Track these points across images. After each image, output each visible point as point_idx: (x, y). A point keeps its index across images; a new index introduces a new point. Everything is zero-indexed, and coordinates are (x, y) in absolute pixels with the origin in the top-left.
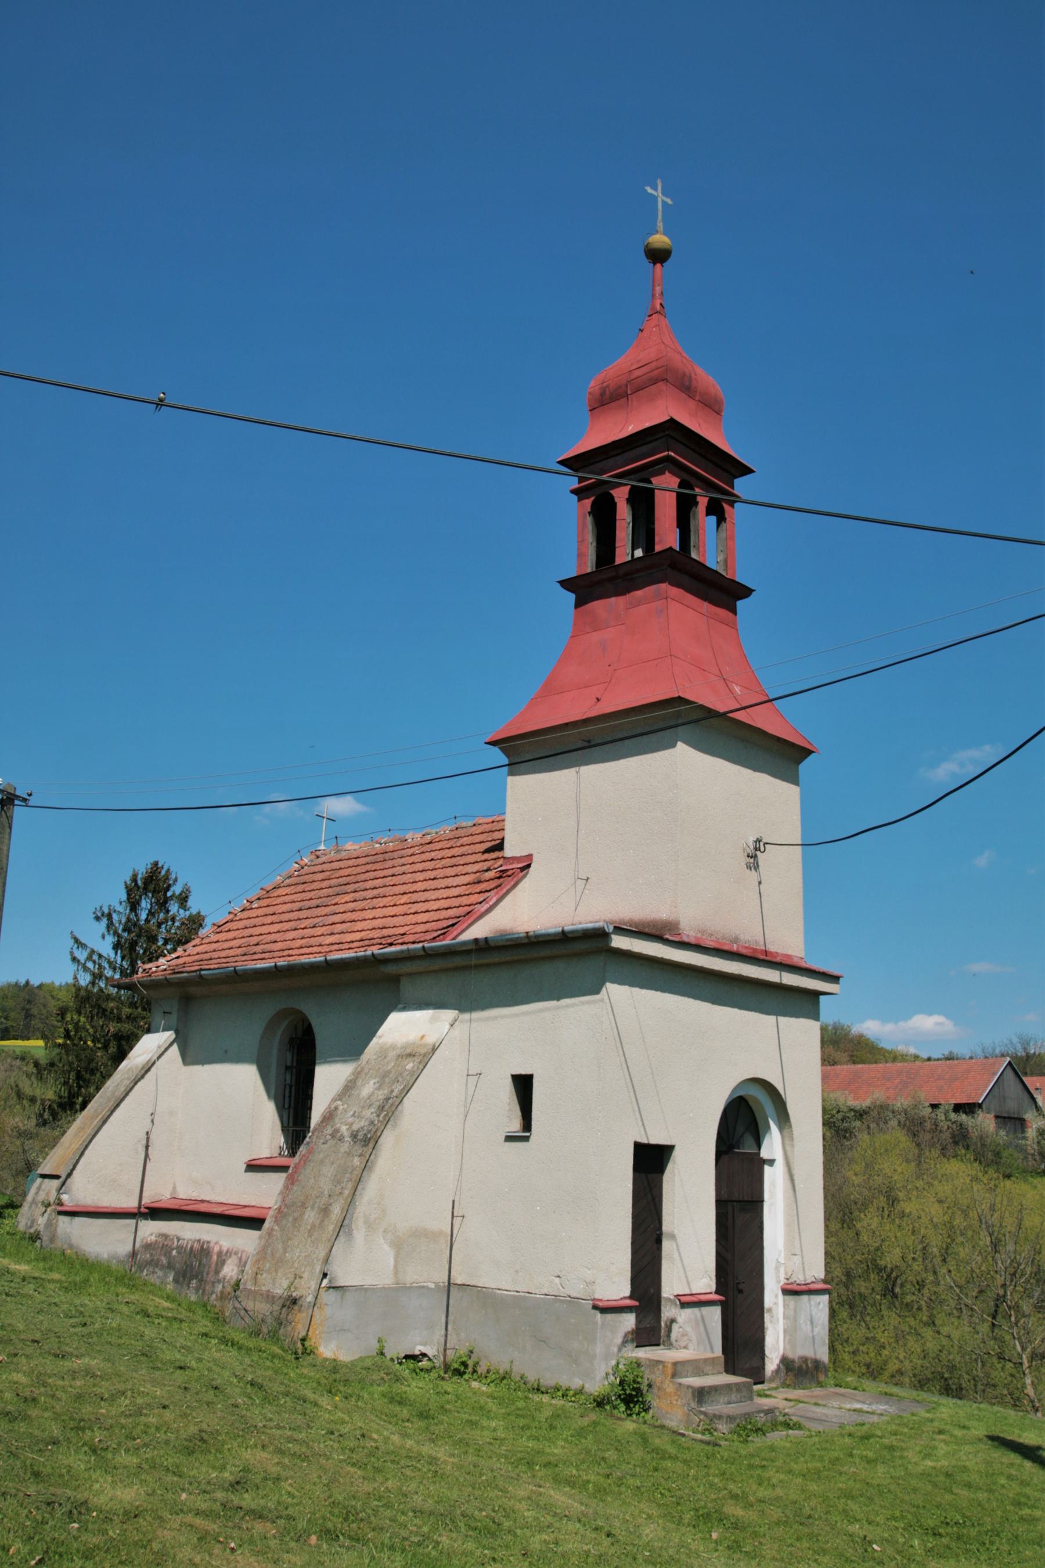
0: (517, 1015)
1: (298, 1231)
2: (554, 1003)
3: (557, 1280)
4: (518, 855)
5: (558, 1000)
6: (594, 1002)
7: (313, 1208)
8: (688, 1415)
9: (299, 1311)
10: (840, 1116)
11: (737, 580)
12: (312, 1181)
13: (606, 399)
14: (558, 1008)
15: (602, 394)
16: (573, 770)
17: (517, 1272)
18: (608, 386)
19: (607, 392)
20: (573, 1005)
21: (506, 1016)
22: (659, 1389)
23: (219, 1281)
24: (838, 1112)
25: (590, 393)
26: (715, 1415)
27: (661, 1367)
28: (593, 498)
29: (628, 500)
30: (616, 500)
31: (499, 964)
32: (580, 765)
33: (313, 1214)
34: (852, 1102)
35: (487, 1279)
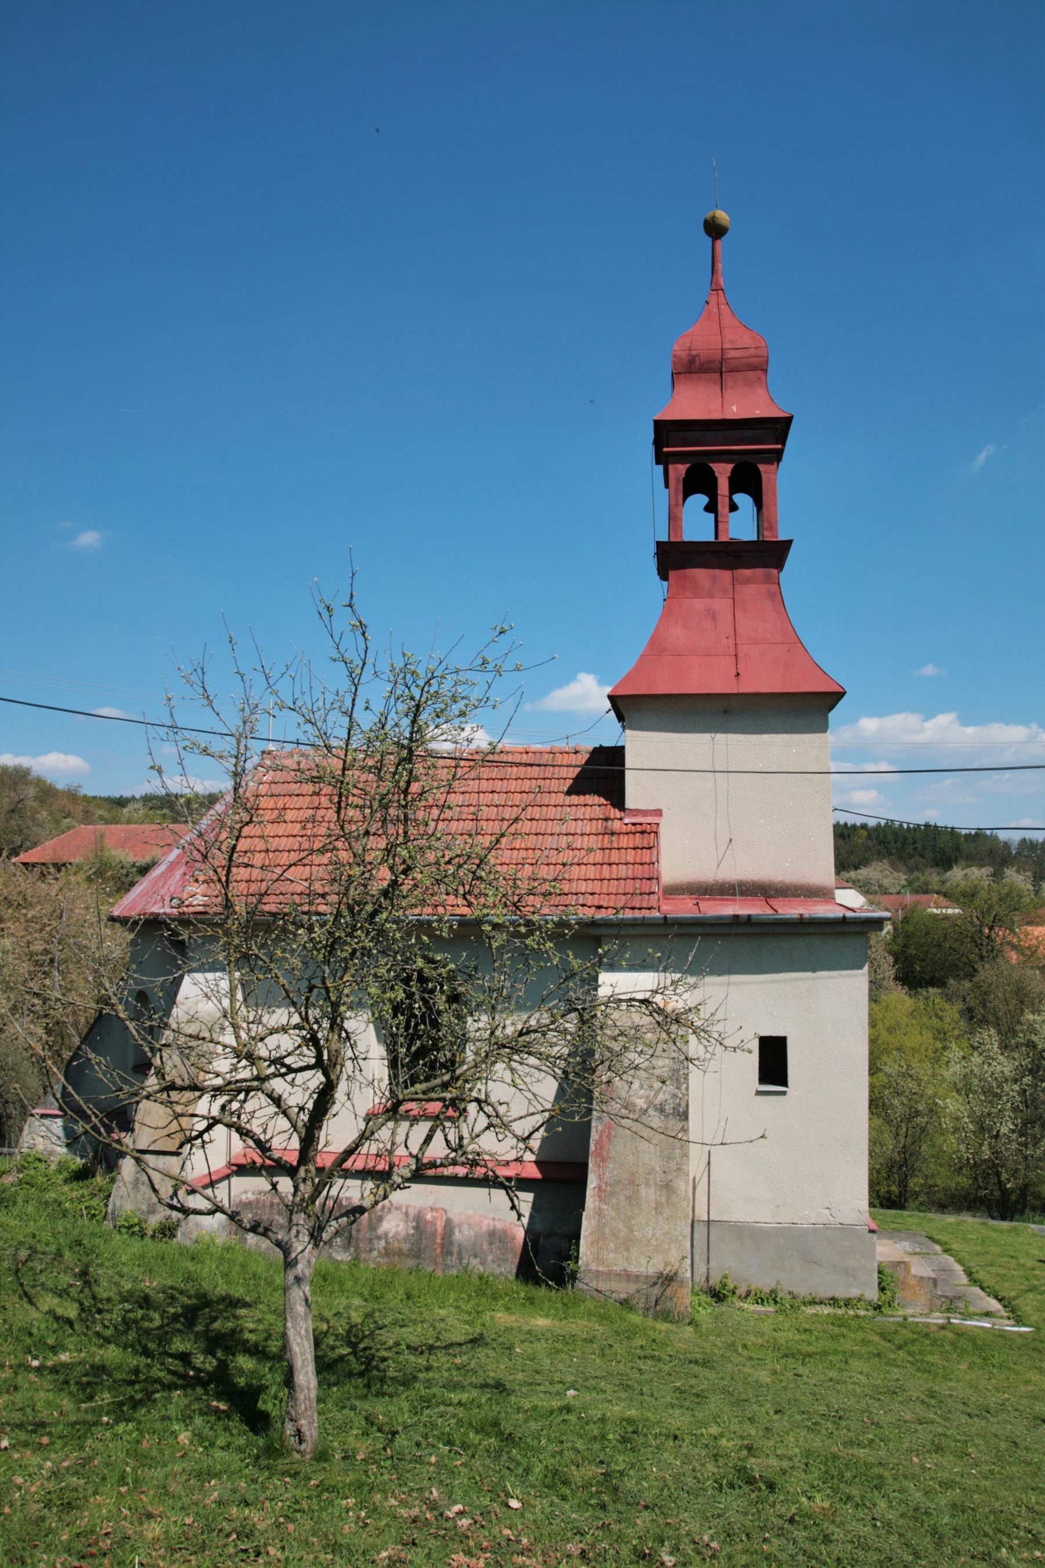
0: (762, 982)
1: (640, 1209)
2: (809, 974)
3: (826, 1212)
4: (644, 808)
5: (814, 971)
6: (856, 976)
7: (647, 1184)
8: (931, 1300)
9: (681, 1287)
10: (124, 872)
11: (686, 540)
12: (631, 1158)
13: (690, 368)
14: (814, 978)
15: (692, 361)
16: (708, 736)
17: (777, 1207)
18: (697, 355)
19: (697, 362)
20: (833, 977)
21: (749, 983)
22: (902, 1283)
23: (379, 1238)
24: (122, 868)
25: (675, 356)
26: (954, 1297)
27: (903, 1266)
28: (688, 465)
29: (730, 479)
30: (717, 474)
31: (744, 934)
32: (716, 732)
33: (652, 1191)
34: (130, 858)
35: (741, 1213)
